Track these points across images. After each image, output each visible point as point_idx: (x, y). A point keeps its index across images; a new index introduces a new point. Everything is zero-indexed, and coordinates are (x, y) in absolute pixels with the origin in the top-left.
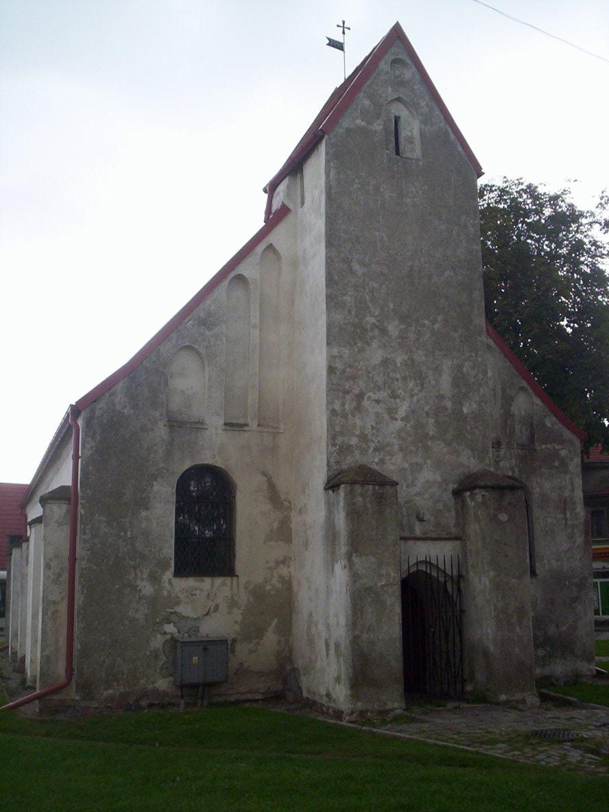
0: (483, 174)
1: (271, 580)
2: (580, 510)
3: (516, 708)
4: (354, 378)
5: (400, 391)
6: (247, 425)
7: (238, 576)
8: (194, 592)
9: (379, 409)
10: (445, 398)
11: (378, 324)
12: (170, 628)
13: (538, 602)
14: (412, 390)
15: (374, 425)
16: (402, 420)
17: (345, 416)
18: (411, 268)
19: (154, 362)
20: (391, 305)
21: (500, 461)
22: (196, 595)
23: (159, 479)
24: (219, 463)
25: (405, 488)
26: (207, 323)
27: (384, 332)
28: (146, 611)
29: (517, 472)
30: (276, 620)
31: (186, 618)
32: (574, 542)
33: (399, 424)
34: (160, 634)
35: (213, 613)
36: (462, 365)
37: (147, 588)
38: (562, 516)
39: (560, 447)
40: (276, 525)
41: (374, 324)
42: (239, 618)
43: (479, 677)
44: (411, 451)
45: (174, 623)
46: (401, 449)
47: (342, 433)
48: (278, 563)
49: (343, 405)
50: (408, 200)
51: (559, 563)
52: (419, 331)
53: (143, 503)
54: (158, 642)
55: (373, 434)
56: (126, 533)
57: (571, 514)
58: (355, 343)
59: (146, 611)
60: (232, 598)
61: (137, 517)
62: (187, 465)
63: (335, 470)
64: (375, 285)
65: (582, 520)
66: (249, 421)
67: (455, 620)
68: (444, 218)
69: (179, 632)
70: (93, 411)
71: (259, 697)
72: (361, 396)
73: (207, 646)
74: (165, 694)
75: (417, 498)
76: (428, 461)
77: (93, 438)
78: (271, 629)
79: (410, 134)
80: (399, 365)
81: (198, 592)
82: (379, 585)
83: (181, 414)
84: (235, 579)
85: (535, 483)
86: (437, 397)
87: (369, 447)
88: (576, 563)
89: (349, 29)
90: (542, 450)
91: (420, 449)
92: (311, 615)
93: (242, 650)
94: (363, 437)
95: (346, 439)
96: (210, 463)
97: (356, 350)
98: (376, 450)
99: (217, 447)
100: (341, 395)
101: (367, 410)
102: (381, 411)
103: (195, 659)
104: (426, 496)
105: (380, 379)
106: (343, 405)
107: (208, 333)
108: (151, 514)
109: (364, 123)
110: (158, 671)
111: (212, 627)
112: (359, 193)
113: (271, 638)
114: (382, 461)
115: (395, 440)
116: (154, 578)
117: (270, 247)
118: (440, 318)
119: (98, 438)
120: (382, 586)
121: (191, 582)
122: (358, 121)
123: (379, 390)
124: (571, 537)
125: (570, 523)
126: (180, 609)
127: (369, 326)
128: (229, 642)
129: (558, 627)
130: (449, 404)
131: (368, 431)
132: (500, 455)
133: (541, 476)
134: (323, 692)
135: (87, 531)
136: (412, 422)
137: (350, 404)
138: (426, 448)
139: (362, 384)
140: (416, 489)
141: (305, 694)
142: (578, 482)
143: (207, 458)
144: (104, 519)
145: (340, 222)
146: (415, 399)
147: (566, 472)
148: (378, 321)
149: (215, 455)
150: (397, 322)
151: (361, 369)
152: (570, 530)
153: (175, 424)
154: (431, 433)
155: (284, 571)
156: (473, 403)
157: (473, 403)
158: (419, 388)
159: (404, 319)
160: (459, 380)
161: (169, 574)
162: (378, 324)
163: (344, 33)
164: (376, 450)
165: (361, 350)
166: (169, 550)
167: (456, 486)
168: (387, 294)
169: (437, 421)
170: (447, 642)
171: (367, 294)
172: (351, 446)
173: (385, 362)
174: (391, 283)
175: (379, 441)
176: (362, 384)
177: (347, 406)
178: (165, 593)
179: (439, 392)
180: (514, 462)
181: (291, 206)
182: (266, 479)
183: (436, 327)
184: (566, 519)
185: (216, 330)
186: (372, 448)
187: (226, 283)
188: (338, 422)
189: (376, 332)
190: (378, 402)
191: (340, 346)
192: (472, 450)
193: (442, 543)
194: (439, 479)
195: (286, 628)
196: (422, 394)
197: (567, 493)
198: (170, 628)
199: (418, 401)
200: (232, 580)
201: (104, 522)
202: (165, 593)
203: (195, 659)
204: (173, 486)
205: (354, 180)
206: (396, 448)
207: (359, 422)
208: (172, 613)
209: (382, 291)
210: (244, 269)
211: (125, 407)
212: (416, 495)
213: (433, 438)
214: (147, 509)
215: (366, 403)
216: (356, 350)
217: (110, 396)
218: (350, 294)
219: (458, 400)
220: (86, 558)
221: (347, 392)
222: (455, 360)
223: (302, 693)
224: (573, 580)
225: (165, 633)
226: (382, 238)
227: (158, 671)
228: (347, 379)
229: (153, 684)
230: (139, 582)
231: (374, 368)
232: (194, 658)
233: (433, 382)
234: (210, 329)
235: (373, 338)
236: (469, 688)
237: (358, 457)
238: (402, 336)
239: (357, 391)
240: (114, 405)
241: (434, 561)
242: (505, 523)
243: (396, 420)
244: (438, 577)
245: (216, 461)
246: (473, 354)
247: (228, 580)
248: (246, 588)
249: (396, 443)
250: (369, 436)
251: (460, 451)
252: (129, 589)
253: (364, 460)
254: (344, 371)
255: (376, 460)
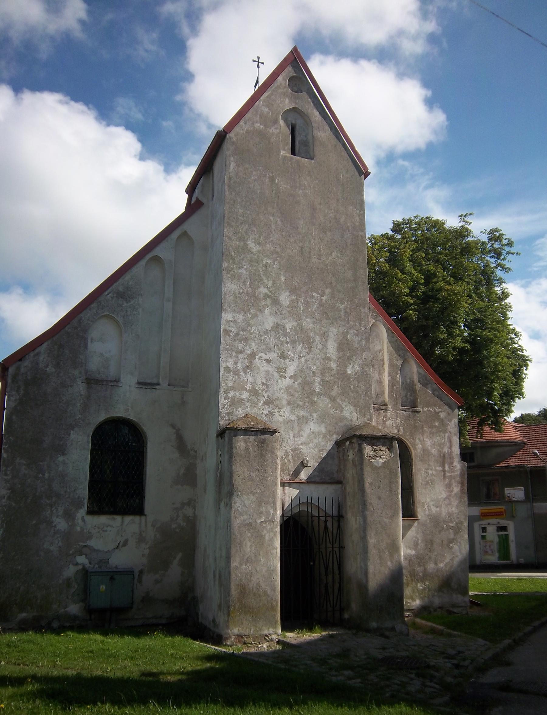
0: (370, 173)
1: (176, 519)
2: (458, 465)
3: (382, 635)
4: (245, 340)
5: (289, 353)
6: (158, 384)
7: (146, 515)
8: (105, 528)
9: (270, 368)
10: (331, 360)
11: (270, 294)
12: (82, 560)
13: (419, 542)
14: (300, 352)
15: (265, 382)
16: (291, 377)
17: (237, 373)
18: (302, 248)
19: (76, 328)
20: (283, 279)
21: (386, 421)
22: (106, 531)
23: (76, 429)
24: (131, 416)
25: (291, 437)
26: (125, 295)
27: (276, 302)
28: (60, 544)
29: (402, 430)
30: (180, 555)
31: (95, 550)
32: (452, 491)
33: (287, 382)
34: (73, 564)
35: (122, 546)
36: (348, 333)
37: (61, 524)
38: (441, 469)
39: (440, 410)
40: (182, 471)
41: (266, 294)
42: (147, 552)
43: (354, 606)
44: (298, 405)
45: (86, 555)
46: (289, 403)
47: (233, 388)
48: (183, 504)
49: (236, 363)
50: (301, 191)
51: (438, 509)
52: (308, 302)
53: (61, 449)
54: (70, 571)
55: (264, 389)
56: (44, 475)
57: (449, 467)
58: (249, 310)
59: (60, 544)
60: (140, 534)
61: (54, 461)
62: (102, 417)
63: (226, 420)
64: (269, 261)
65: (459, 473)
66: (161, 381)
67: (335, 555)
68: (333, 208)
69: (90, 563)
70: (18, 368)
71: (164, 621)
72: (252, 356)
73: (113, 575)
74: (76, 617)
75: (302, 447)
76: (315, 415)
77: (17, 391)
78: (176, 562)
79: (305, 139)
80: (288, 331)
81: (109, 529)
82: (259, 521)
83: (99, 373)
84: (143, 518)
85: (417, 440)
86: (323, 359)
87: (259, 401)
88: (454, 509)
89: (263, 63)
90: (424, 412)
91: (307, 404)
92: (205, 550)
93: (148, 580)
94: (254, 392)
95: (238, 394)
96: (123, 416)
97: (250, 316)
98: (267, 403)
99: (129, 402)
100: (234, 354)
101: (259, 368)
102: (271, 369)
103: (103, 588)
104: (311, 445)
105: (271, 342)
106: (236, 363)
107: (125, 304)
108: (68, 459)
109: (262, 126)
110: (70, 597)
111: (120, 560)
112: (257, 184)
113: (175, 571)
114: (271, 414)
115: (284, 395)
116: (69, 516)
117: (185, 234)
118: (327, 291)
119: (22, 392)
120: (261, 522)
121: (103, 519)
122: (257, 125)
123: (270, 350)
124: (449, 486)
125: (448, 474)
126: (92, 543)
127: (262, 296)
128: (136, 574)
129: (436, 564)
130: (334, 366)
131: (259, 387)
132: (386, 415)
133: (423, 434)
134: (211, 618)
135: (8, 473)
136: (300, 380)
137: (242, 362)
138: (313, 403)
139: (254, 345)
140: (303, 439)
141: (200, 620)
142: (456, 440)
143: (119, 412)
144: (25, 462)
145: (238, 207)
146: (303, 360)
147: (445, 431)
148: (270, 292)
149: (128, 409)
150: (288, 293)
151: (254, 333)
152: (447, 481)
153: (91, 381)
154: (317, 390)
155: (189, 511)
156: (356, 366)
157: (356, 366)
158: (307, 350)
159: (293, 291)
160: (344, 346)
161: (82, 512)
162: (270, 294)
163: (258, 67)
164: (267, 403)
165: (255, 316)
166: (83, 490)
167: (339, 437)
168: (280, 269)
169: (323, 381)
170: (327, 575)
171: (262, 268)
172: (243, 399)
173: (277, 327)
174: (283, 260)
175: (268, 395)
176: (254, 345)
177: (239, 365)
178: (78, 529)
179: (325, 354)
180: (399, 422)
181: (204, 200)
182: (174, 431)
183: (324, 298)
184: (444, 471)
185: (133, 302)
186: (262, 402)
187: (143, 263)
188: (230, 378)
189: (269, 301)
190: (268, 361)
191: (234, 311)
192: (355, 406)
193: (326, 486)
194: (324, 430)
195: (189, 562)
196: (310, 356)
197: (446, 450)
198: (82, 560)
199: (306, 361)
200: (140, 520)
201: (25, 465)
202: (78, 529)
203: (103, 588)
204: (89, 436)
205: (252, 172)
206: (284, 402)
207: (250, 379)
208: (84, 546)
209: (275, 266)
210: (163, 252)
211: (48, 366)
212: (302, 444)
213: (319, 394)
214: (63, 454)
215: (257, 361)
216: (250, 316)
217: (34, 356)
218: (245, 267)
219: (344, 360)
220: (6, 496)
221: (241, 352)
222: (340, 328)
223: (198, 619)
224: (451, 524)
225: (77, 564)
226: (277, 222)
227: (70, 597)
228: (241, 341)
229: (65, 609)
230: (54, 519)
231: (266, 332)
232: (101, 587)
233: (320, 346)
234: (127, 302)
235: (265, 306)
236: (346, 616)
237: (249, 409)
238: (293, 305)
239: (249, 352)
240: (37, 364)
241: (315, 502)
242: (379, 468)
243: (285, 377)
244: (319, 516)
245: (129, 415)
246: (357, 324)
247: (137, 518)
248: (153, 526)
249: (285, 398)
250: (260, 391)
251: (344, 406)
252: (44, 524)
253: (254, 412)
254: (237, 334)
255: (266, 412)
